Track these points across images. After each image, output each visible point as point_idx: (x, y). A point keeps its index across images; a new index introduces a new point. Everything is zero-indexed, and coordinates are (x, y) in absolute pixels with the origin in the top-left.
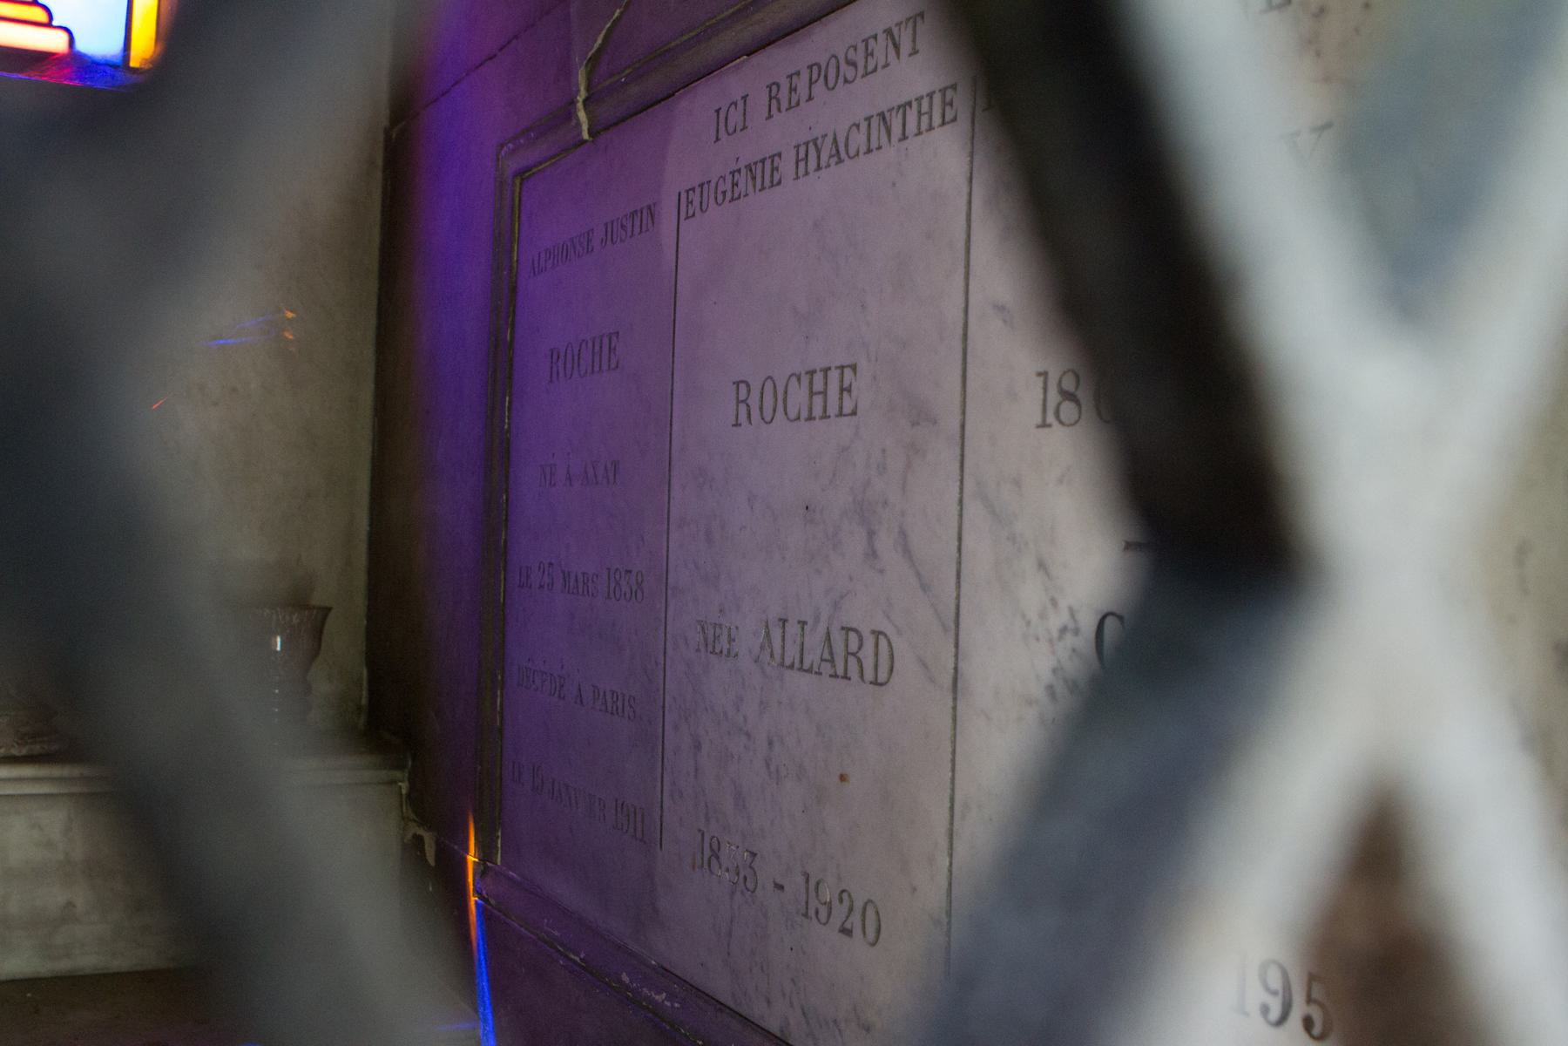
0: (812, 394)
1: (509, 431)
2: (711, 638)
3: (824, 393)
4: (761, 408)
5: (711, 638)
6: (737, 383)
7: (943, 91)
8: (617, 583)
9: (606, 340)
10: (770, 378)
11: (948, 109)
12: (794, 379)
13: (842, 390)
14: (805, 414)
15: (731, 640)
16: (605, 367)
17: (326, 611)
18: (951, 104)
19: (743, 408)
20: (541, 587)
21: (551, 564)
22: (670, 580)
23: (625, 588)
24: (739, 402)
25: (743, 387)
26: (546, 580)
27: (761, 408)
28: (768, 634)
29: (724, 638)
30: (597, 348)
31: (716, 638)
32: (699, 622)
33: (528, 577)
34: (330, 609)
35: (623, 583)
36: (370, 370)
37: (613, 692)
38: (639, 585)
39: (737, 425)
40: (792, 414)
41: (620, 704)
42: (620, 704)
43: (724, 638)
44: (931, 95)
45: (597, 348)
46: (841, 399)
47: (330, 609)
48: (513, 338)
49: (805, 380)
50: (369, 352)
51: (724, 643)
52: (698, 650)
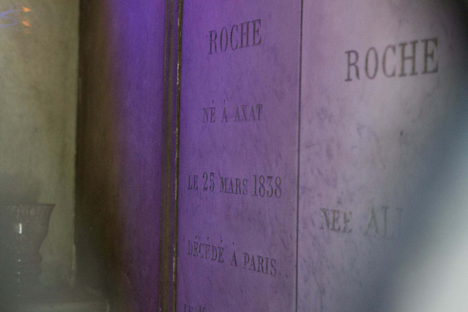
0: (404, 58)
1: (180, 85)
2: (331, 221)
3: (413, 58)
4: (366, 69)
5: (331, 221)
6: (349, 53)
7: (426, 41)
8: (262, 185)
9: (251, 26)
10: (373, 48)
11: (429, 59)
12: (390, 51)
13: (426, 56)
14: (398, 72)
15: (346, 221)
16: (251, 43)
17: (52, 206)
18: (432, 55)
19: (353, 69)
20: (205, 189)
21: (212, 174)
22: (301, 183)
23: (267, 188)
24: (350, 65)
25: (353, 56)
26: (209, 184)
27: (366, 69)
28: (374, 217)
29: (341, 221)
30: (245, 31)
31: (335, 220)
32: (323, 210)
33: (195, 182)
34: (53, 206)
35: (266, 185)
36: (75, 45)
37: (259, 257)
38: (278, 186)
39: (349, 80)
40: (389, 72)
41: (264, 264)
42: (264, 264)
43: (341, 221)
44: (414, 43)
45: (245, 31)
46: (426, 61)
47: (53, 206)
48: (181, 23)
49: (399, 49)
50: (74, 34)
51: (341, 222)
52: (322, 228)
